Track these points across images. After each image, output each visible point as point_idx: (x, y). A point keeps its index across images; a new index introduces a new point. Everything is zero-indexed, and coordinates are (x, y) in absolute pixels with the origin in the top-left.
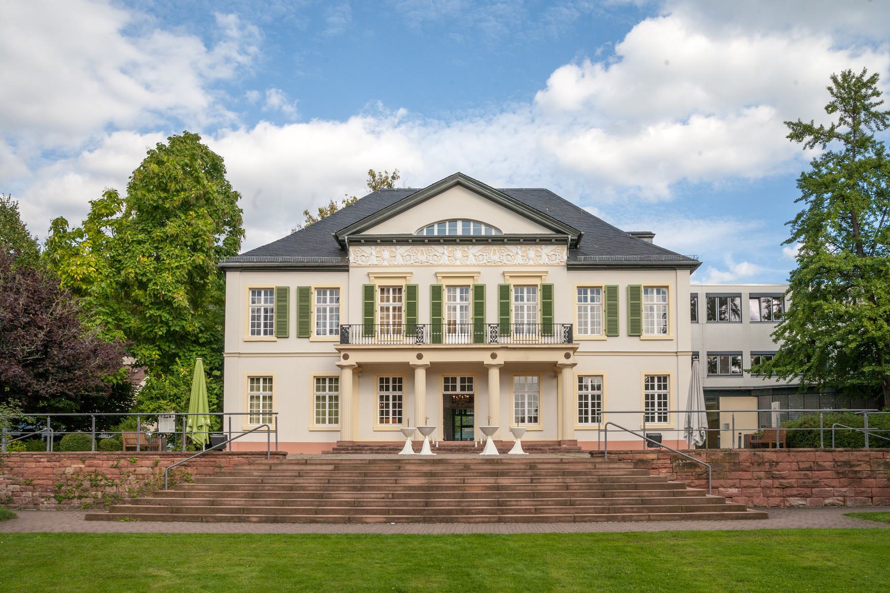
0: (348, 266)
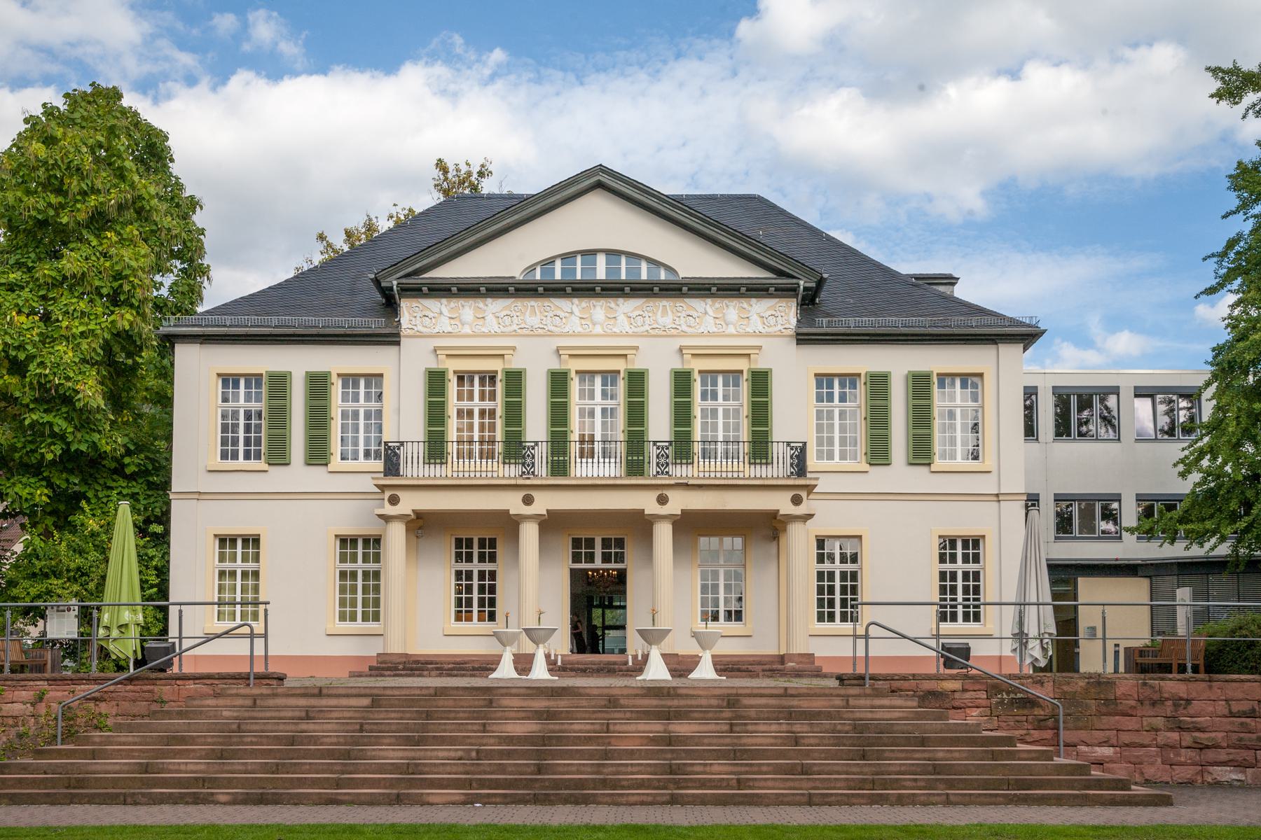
0: (398, 335)
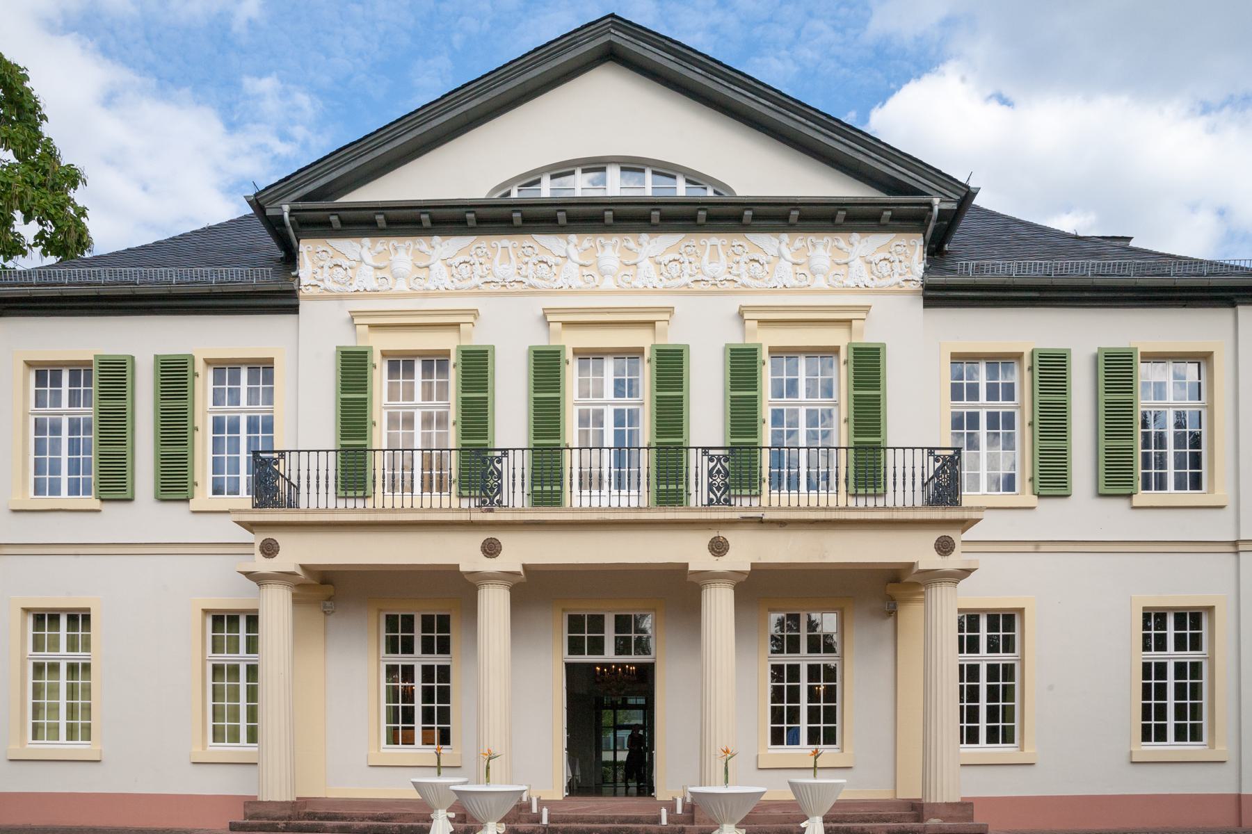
0: (292, 294)
